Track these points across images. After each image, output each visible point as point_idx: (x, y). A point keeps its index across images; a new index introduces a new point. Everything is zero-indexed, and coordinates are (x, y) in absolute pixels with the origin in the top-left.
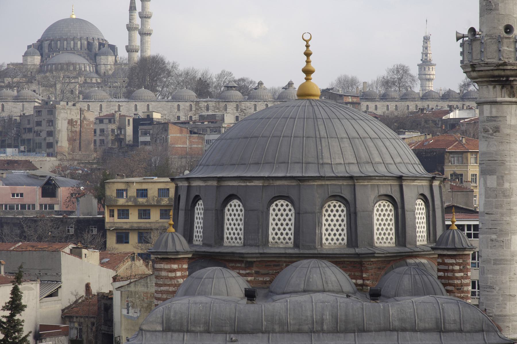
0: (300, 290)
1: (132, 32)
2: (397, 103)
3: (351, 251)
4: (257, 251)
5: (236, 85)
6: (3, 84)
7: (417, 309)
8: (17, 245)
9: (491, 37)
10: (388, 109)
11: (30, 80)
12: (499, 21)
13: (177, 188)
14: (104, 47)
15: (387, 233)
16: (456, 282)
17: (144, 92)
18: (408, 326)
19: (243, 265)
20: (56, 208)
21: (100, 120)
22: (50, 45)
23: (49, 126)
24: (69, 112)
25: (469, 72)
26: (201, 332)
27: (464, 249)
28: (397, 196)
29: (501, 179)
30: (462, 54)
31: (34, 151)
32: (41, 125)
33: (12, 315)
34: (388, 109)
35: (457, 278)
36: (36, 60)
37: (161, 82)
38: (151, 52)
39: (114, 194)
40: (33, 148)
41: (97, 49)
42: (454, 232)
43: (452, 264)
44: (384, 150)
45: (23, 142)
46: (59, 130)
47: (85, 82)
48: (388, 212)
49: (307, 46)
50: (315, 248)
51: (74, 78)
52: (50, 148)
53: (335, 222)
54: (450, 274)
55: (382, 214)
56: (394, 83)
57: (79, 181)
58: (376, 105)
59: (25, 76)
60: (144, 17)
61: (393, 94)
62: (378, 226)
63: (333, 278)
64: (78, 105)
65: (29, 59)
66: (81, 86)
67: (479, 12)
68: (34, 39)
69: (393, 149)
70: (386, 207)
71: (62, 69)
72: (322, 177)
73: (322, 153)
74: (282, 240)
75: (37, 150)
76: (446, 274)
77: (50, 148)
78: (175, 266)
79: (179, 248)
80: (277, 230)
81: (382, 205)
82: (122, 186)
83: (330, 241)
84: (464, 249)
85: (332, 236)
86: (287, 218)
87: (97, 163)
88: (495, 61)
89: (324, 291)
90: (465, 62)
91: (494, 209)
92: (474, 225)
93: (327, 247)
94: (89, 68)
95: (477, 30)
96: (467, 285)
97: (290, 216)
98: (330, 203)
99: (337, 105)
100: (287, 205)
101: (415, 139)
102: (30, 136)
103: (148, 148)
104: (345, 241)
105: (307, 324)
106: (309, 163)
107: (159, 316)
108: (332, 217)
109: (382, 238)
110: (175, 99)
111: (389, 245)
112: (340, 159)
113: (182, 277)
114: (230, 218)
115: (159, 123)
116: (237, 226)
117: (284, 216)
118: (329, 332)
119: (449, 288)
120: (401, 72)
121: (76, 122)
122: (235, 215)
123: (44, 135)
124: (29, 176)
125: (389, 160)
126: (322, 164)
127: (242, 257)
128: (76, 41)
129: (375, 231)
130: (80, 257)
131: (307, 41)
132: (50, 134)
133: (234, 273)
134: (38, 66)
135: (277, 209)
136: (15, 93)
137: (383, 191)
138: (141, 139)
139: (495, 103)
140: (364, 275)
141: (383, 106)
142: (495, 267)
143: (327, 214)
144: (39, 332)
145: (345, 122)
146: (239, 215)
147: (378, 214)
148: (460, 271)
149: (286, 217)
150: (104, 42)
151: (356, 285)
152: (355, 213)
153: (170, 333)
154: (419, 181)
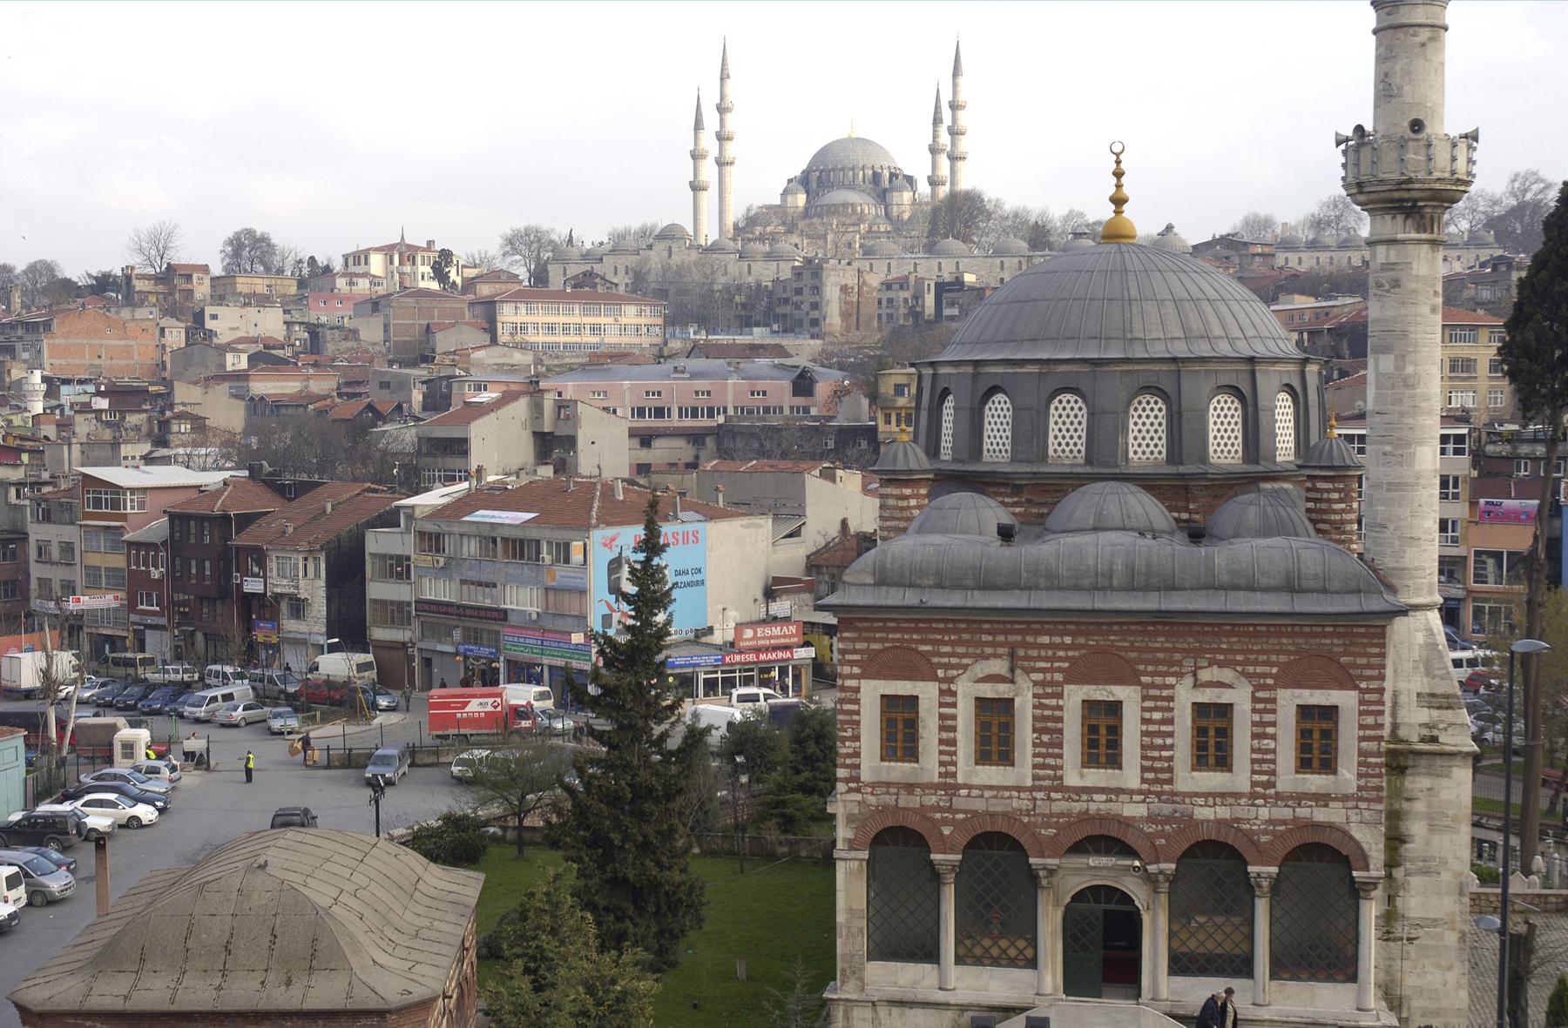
3: (1172, 470)
9: (1388, 138)
13: (920, 377)
16: (1333, 517)
17: (951, 243)
18: (1242, 582)
20: (814, 411)
21: (888, 286)
22: (819, 178)
26: (930, 587)
27: (1348, 468)
28: (1245, 388)
29: (1401, 360)
30: (1344, 166)
33: (649, 559)
35: (1335, 512)
37: (978, 228)
38: (964, 185)
39: (892, 392)
43: (1328, 491)
44: (1229, 318)
45: (777, 318)
47: (870, 231)
49: (1118, 162)
54: (1324, 506)
56: (1329, 224)
59: (784, 223)
60: (954, 133)
63: (1139, 509)
64: (855, 265)
65: (790, 198)
68: (797, 170)
78: (908, 491)
79: (913, 465)
82: (902, 380)
87: (882, 348)
88: (1396, 176)
89: (1124, 529)
95: (1369, 127)
96: (1351, 522)
102: (786, 309)
112: (1160, 334)
113: (918, 507)
115: (972, 289)
118: (1121, 589)
119: (1322, 526)
123: (806, 307)
125: (1237, 333)
129: (1211, 440)
130: (834, 481)
132: (815, 306)
136: (767, 248)
137: (1223, 381)
138: (947, 312)
139: (1393, 242)
142: (1390, 495)
145: (1170, 276)
148: (1340, 501)
151: (1177, 520)
152: (1180, 413)
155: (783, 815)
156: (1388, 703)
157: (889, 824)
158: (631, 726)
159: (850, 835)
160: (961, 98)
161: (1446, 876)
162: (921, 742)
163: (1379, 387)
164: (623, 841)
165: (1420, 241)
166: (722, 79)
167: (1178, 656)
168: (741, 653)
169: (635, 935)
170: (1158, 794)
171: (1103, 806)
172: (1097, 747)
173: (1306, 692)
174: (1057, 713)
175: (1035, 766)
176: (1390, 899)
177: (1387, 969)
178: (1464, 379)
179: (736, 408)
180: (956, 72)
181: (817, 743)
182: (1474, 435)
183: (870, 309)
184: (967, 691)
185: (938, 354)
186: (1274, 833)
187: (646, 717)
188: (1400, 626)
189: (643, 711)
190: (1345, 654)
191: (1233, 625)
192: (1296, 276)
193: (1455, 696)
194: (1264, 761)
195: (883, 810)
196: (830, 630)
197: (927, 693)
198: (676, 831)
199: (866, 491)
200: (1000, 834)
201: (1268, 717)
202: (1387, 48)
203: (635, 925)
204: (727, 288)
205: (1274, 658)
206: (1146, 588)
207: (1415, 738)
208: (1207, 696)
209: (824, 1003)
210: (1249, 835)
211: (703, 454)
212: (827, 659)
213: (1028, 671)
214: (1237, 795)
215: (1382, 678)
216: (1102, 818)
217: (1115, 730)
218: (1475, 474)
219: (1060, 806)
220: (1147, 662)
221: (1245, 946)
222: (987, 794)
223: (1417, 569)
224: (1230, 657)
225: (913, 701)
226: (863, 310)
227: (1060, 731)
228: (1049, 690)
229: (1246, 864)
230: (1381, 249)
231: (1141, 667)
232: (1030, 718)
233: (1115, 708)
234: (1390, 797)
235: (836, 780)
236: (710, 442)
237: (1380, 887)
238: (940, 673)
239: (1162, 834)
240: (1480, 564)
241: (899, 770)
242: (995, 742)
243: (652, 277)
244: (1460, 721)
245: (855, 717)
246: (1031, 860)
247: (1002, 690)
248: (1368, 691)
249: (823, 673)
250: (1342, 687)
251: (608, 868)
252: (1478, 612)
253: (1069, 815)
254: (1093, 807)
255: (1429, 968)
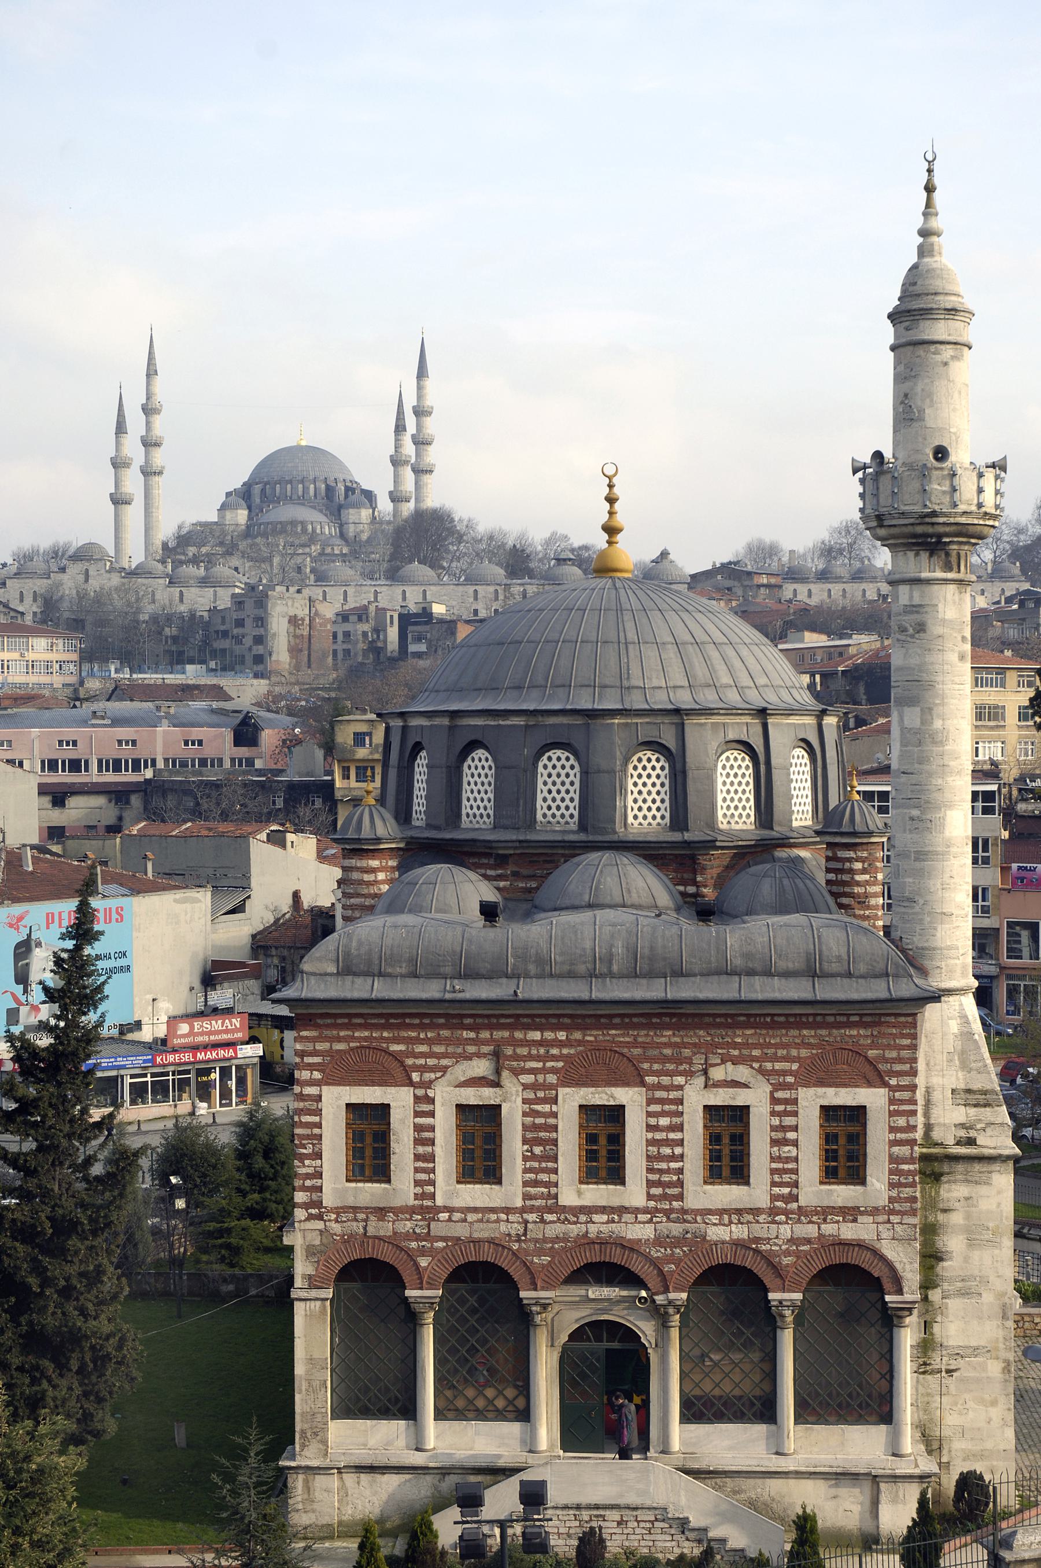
0: (584, 904)
1: (400, 469)
2: (846, 586)
3: (677, 837)
4: (514, 838)
5: (572, 557)
6: (183, 558)
7: (774, 938)
8: (184, 827)
9: (910, 467)
10: (830, 596)
11: (230, 551)
12: (925, 439)
13: (388, 729)
14: (353, 493)
15: (740, 806)
16: (856, 890)
17: (417, 569)
18: (758, 966)
19: (492, 861)
20: (258, 764)
21: (344, 617)
22: (263, 491)
23: (257, 626)
24: (290, 604)
25: (874, 528)
26: (402, 976)
29: (928, 712)
30: (862, 496)
31: (232, 669)
32: (243, 626)
33: (78, 948)
34: (830, 596)
35: (858, 884)
36: (239, 517)
37: (448, 551)
38: (433, 500)
40: (230, 664)
41: (342, 498)
42: (853, 805)
43: (850, 860)
44: (737, 664)
45: (214, 654)
46: (274, 634)
47: (322, 554)
48: (743, 770)
49: (611, 486)
50: (615, 832)
51: (303, 546)
52: (259, 664)
53: (649, 787)
54: (846, 877)
55: (732, 773)
56: (841, 551)
57: (296, 719)
58: (810, 590)
59: (221, 544)
60: (421, 442)
61: (838, 570)
62: (725, 794)
63: (641, 883)
64: (306, 592)
65: (229, 515)
66: (314, 560)
67: (892, 424)
68: (238, 479)
69: (754, 661)
70: (739, 762)
71: (283, 531)
72: (626, 710)
73: (628, 670)
74: (558, 818)
75: (237, 667)
76: (839, 876)
77: (259, 664)
80: (549, 802)
81: (732, 757)
82: (363, 728)
83: (640, 820)
84: (870, 834)
85: (645, 811)
86: (567, 781)
87: (339, 689)
88: (918, 509)
90: (867, 511)
91: (916, 766)
92: (983, 792)
93: (635, 831)
94: (329, 530)
95: (888, 454)
96: (875, 895)
97: (572, 778)
98: (640, 754)
99: (660, 586)
100: (568, 759)
101: (865, 647)
103: (422, 663)
104: (667, 820)
105: (585, 963)
106: (606, 687)
107: (332, 948)
108: (644, 779)
109: (733, 815)
110: (470, 580)
111: (745, 827)
112: (659, 678)
114: (472, 781)
115: (441, 621)
116: (483, 794)
117: (563, 778)
118: (622, 976)
119: (845, 901)
120: (853, 532)
121: (303, 619)
122: (479, 776)
123: (248, 641)
124: (213, 711)
125: (746, 681)
126: (628, 688)
127: (491, 848)
128: (307, 484)
129: (720, 803)
130: (283, 846)
131: (610, 478)
132: (259, 640)
133: (472, 875)
134: (243, 527)
135: (550, 765)
136: (202, 572)
137: (731, 736)
138: (412, 648)
140: (699, 879)
141: (822, 590)
143: (635, 774)
144: (210, 972)
145: (671, 616)
146: (486, 776)
147: (724, 773)
148: (864, 871)
149: (565, 780)
150: (355, 485)
151: (683, 894)
152: (684, 772)
153: (350, 978)
154: (797, 717)
155: (228, 1246)
156: (921, 1102)
157: (357, 1256)
158: (55, 1147)
159: (310, 1270)
160: (429, 402)
161: (988, 1298)
162: (394, 1159)
163: (904, 743)
164: (42, 1286)
165: (946, 581)
166: (148, 375)
167: (687, 1052)
168: (174, 1051)
169: (54, 1399)
170: (667, 1213)
171: (604, 1228)
172: (596, 1160)
173: (831, 1091)
174: (551, 1121)
175: (526, 1184)
176: (927, 1326)
177: (922, 1405)
178: (992, 728)
179: (166, 760)
180: (422, 372)
181: (266, 1156)
182: (1004, 791)
183: (323, 643)
184: (446, 1097)
185: (408, 705)
186: (798, 1254)
187: (69, 1136)
188: (931, 1013)
189: (67, 1128)
190: (872, 1046)
191: (748, 1016)
192: (805, 610)
193: (993, 1092)
194: (784, 1171)
195: (348, 1239)
196: (281, 1023)
197: (399, 1099)
198: (104, 1272)
199: (322, 857)
200: (486, 1264)
201: (789, 1121)
202: (906, 366)
203: (54, 1387)
204: (155, 619)
205: (794, 1052)
206: (651, 975)
207: (951, 1141)
208: (720, 1098)
209: (282, 1472)
210: (767, 1259)
211: (127, 815)
212: (277, 1058)
213: (516, 1073)
214: (755, 1212)
215: (914, 1073)
216: (602, 1243)
217: (617, 1140)
218: (1005, 835)
219: (554, 1230)
220: (652, 1060)
221: (766, 1387)
222: (471, 1217)
223: (949, 948)
224: (745, 1052)
225: (384, 1110)
226: (316, 646)
227: (555, 1142)
228: (541, 1094)
229: (766, 1291)
230: (904, 589)
231: (646, 1066)
232: (520, 1127)
233: (616, 1114)
234: (924, 1208)
235: (295, 1206)
236: (136, 800)
237: (915, 1312)
238: (415, 1077)
239: (670, 1259)
240: (1014, 937)
241: (369, 1192)
242: (481, 1160)
243: (65, 605)
244: (999, 1120)
245: (316, 1131)
246: (523, 1294)
247: (486, 1096)
248: (899, 1088)
249: (275, 1075)
250: (870, 1084)
251: (23, 1320)
252: (1012, 991)
253: (565, 1239)
254: (593, 1229)
255: (971, 1404)
